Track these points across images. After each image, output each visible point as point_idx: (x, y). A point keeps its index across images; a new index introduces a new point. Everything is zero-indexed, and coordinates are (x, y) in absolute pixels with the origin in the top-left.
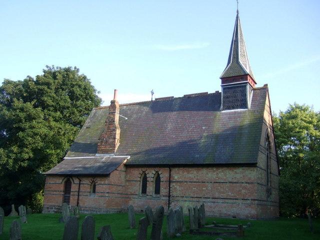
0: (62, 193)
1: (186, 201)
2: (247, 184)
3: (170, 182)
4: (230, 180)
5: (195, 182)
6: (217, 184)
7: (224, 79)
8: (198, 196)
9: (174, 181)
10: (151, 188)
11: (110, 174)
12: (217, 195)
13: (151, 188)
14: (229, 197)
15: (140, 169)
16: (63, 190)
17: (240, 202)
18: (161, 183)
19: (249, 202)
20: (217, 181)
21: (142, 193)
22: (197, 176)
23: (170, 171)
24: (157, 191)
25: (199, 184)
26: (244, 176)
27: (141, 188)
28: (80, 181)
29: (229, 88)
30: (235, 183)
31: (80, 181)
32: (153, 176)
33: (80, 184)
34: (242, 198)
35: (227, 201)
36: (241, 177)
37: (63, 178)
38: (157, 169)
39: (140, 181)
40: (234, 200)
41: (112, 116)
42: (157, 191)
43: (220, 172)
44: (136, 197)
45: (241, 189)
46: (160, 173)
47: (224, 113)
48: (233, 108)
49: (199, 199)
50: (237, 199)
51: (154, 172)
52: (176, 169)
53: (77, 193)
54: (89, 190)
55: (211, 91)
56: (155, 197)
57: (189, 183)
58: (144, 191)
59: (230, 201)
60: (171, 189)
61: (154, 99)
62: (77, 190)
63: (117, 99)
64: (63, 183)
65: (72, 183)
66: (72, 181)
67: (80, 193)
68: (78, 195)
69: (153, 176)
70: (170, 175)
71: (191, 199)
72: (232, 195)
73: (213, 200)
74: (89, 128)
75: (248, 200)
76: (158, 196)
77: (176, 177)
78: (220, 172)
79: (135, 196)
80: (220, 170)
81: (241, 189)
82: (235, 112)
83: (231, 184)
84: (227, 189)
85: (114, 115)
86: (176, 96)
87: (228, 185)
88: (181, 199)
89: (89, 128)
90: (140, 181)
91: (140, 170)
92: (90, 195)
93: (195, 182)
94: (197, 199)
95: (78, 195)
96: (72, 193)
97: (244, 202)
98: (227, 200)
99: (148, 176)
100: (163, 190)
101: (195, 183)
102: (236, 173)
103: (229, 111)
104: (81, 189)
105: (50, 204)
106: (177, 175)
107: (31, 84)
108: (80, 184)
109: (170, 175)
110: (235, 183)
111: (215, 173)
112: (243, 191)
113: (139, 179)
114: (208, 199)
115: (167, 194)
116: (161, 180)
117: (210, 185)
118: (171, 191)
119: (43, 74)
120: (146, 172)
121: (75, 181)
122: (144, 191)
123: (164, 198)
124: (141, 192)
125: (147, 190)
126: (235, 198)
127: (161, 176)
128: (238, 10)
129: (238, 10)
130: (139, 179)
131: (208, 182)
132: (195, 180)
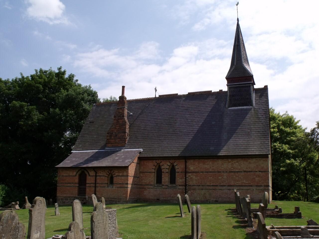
0: (77, 185)
1: (202, 189)
2: (260, 173)
3: (186, 172)
4: (245, 169)
5: (210, 172)
6: (233, 174)
7: (229, 78)
8: (214, 184)
9: (190, 171)
10: (166, 178)
11: (128, 166)
12: (232, 183)
13: (166, 178)
14: (244, 185)
15: (154, 161)
16: (77, 182)
17: (254, 188)
18: (177, 174)
19: (262, 188)
20: (232, 171)
21: (157, 183)
22: (213, 166)
23: (186, 162)
24: (173, 180)
25: (215, 173)
26: (257, 166)
27: (156, 179)
28: (96, 173)
29: (232, 87)
30: (250, 172)
31: (96, 173)
32: (168, 167)
33: (96, 176)
34: (256, 184)
35: (242, 187)
36: (255, 167)
37: (77, 171)
38: (172, 161)
39: (154, 172)
40: (249, 187)
41: (121, 111)
42: (173, 180)
43: (235, 163)
44: (152, 187)
45: (255, 177)
46: (175, 164)
47: (231, 110)
48: (239, 106)
49: (216, 187)
50: (251, 186)
51: (169, 164)
52: (192, 161)
53: (94, 185)
54: (106, 182)
55: (215, 89)
56: (170, 187)
57: (205, 173)
58: (159, 180)
59: (245, 188)
60: (187, 179)
61: (157, 96)
62: (94, 182)
63: (126, 95)
64: (78, 175)
65: (88, 175)
66: (87, 173)
67: (97, 185)
68: (95, 187)
69: (168, 167)
70: (186, 166)
71: (208, 187)
72: (247, 182)
73: (229, 188)
74: (93, 122)
75: (262, 186)
76: (174, 185)
77: (192, 168)
78: (235, 163)
79: (150, 186)
80: (235, 161)
81: (255, 177)
82: (242, 109)
83: (246, 173)
84: (242, 178)
85: (123, 110)
86: (180, 93)
87: (243, 174)
88: (197, 187)
89: (93, 122)
90: (154, 172)
91: (155, 162)
92: (108, 187)
93: (210, 172)
94: (214, 188)
95: (95, 187)
96: (87, 185)
97: (258, 188)
98: (242, 187)
99: (162, 167)
100: (179, 180)
101: (211, 173)
102: (250, 163)
103: (236, 108)
104: (98, 181)
105: (65, 195)
106: (192, 166)
107: (18, 80)
108: (96, 176)
109: (186, 166)
110: (250, 172)
111: (230, 164)
112: (257, 179)
113: (153, 171)
114: (224, 187)
115: (94, 182)
116: (177, 171)
117: (225, 174)
118: (187, 181)
119: (57, 71)
120: (161, 164)
121: (90, 173)
122: (159, 180)
123: (181, 187)
124: (155, 182)
125: (163, 181)
126: (249, 185)
127: (176, 167)
128: (238, 19)
129: (238, 19)
130: (153, 171)
131: (223, 172)
132: (211, 170)
